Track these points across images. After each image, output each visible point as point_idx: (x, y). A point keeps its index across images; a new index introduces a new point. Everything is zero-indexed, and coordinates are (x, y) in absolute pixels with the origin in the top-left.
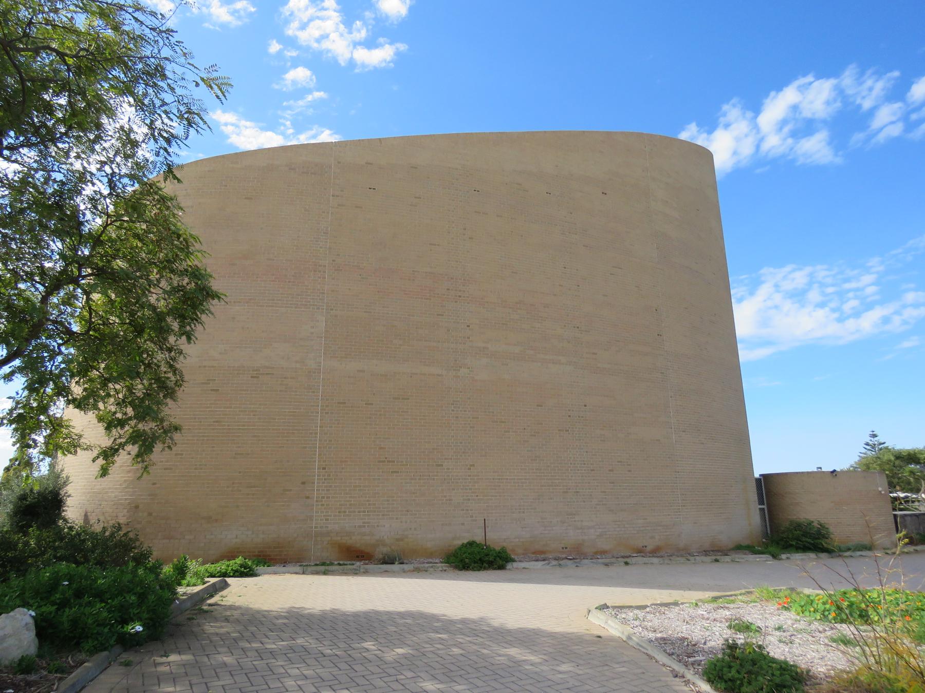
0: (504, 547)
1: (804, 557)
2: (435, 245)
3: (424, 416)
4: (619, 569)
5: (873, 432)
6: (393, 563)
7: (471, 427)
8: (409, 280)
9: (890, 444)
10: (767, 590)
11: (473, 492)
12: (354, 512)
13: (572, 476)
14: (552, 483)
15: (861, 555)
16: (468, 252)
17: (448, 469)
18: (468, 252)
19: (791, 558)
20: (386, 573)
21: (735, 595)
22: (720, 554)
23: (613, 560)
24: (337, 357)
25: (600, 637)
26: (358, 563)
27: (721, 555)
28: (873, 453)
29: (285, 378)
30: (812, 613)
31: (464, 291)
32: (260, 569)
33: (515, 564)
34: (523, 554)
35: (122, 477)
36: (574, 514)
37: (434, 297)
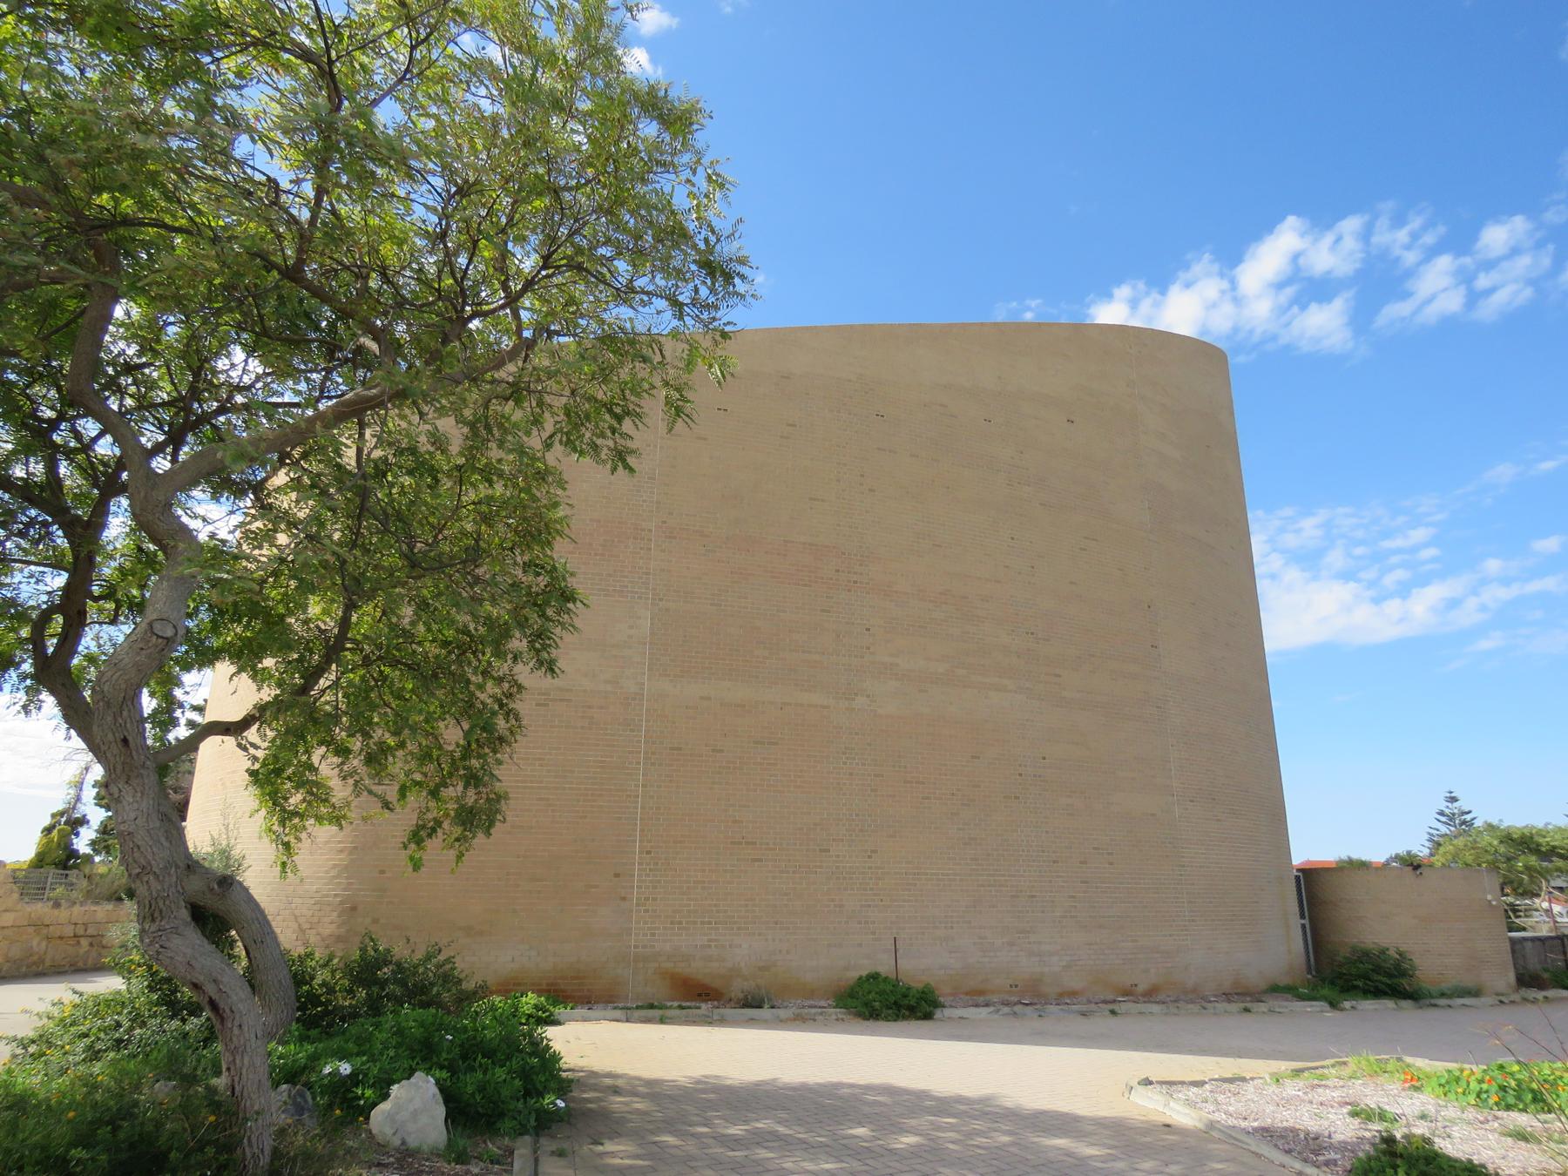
0: (928, 984)
1: (1377, 1006)
2: (818, 500)
3: (801, 771)
4: (1102, 1023)
5: (1451, 792)
6: (760, 1007)
7: (872, 790)
8: (778, 554)
9: (1480, 819)
10: (1368, 1061)
11: (875, 895)
12: (695, 923)
13: (1024, 871)
14: (995, 881)
15: (1464, 1005)
16: (867, 512)
17: (838, 856)
18: (867, 512)
19: (1360, 1007)
20: (751, 1023)
21: (1323, 1067)
22: (1248, 999)
23: (1093, 1007)
24: (669, 675)
25: (1168, 1126)
26: (703, 1006)
27: (1251, 1001)
28: (1453, 829)
29: (590, 707)
30: (1460, 1096)
31: (861, 574)
32: (559, 1011)
33: (947, 1012)
34: (952, 995)
35: (328, 860)
36: (1029, 932)
37: (816, 582)
